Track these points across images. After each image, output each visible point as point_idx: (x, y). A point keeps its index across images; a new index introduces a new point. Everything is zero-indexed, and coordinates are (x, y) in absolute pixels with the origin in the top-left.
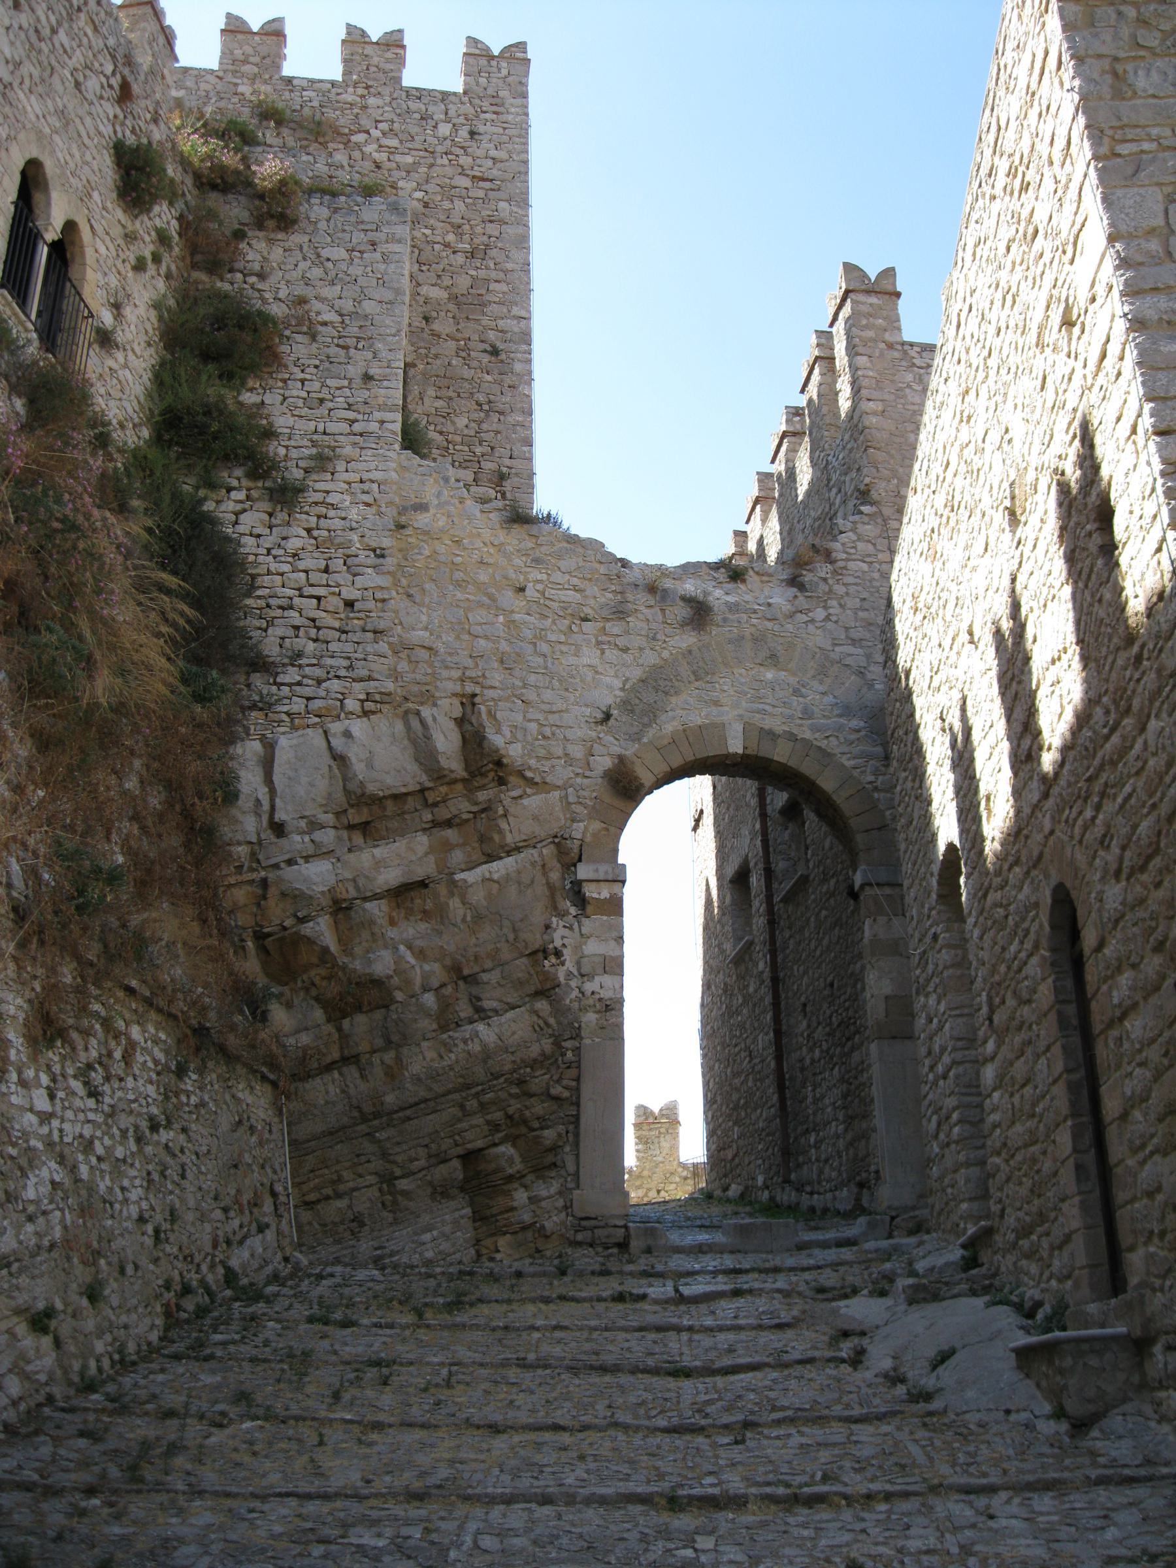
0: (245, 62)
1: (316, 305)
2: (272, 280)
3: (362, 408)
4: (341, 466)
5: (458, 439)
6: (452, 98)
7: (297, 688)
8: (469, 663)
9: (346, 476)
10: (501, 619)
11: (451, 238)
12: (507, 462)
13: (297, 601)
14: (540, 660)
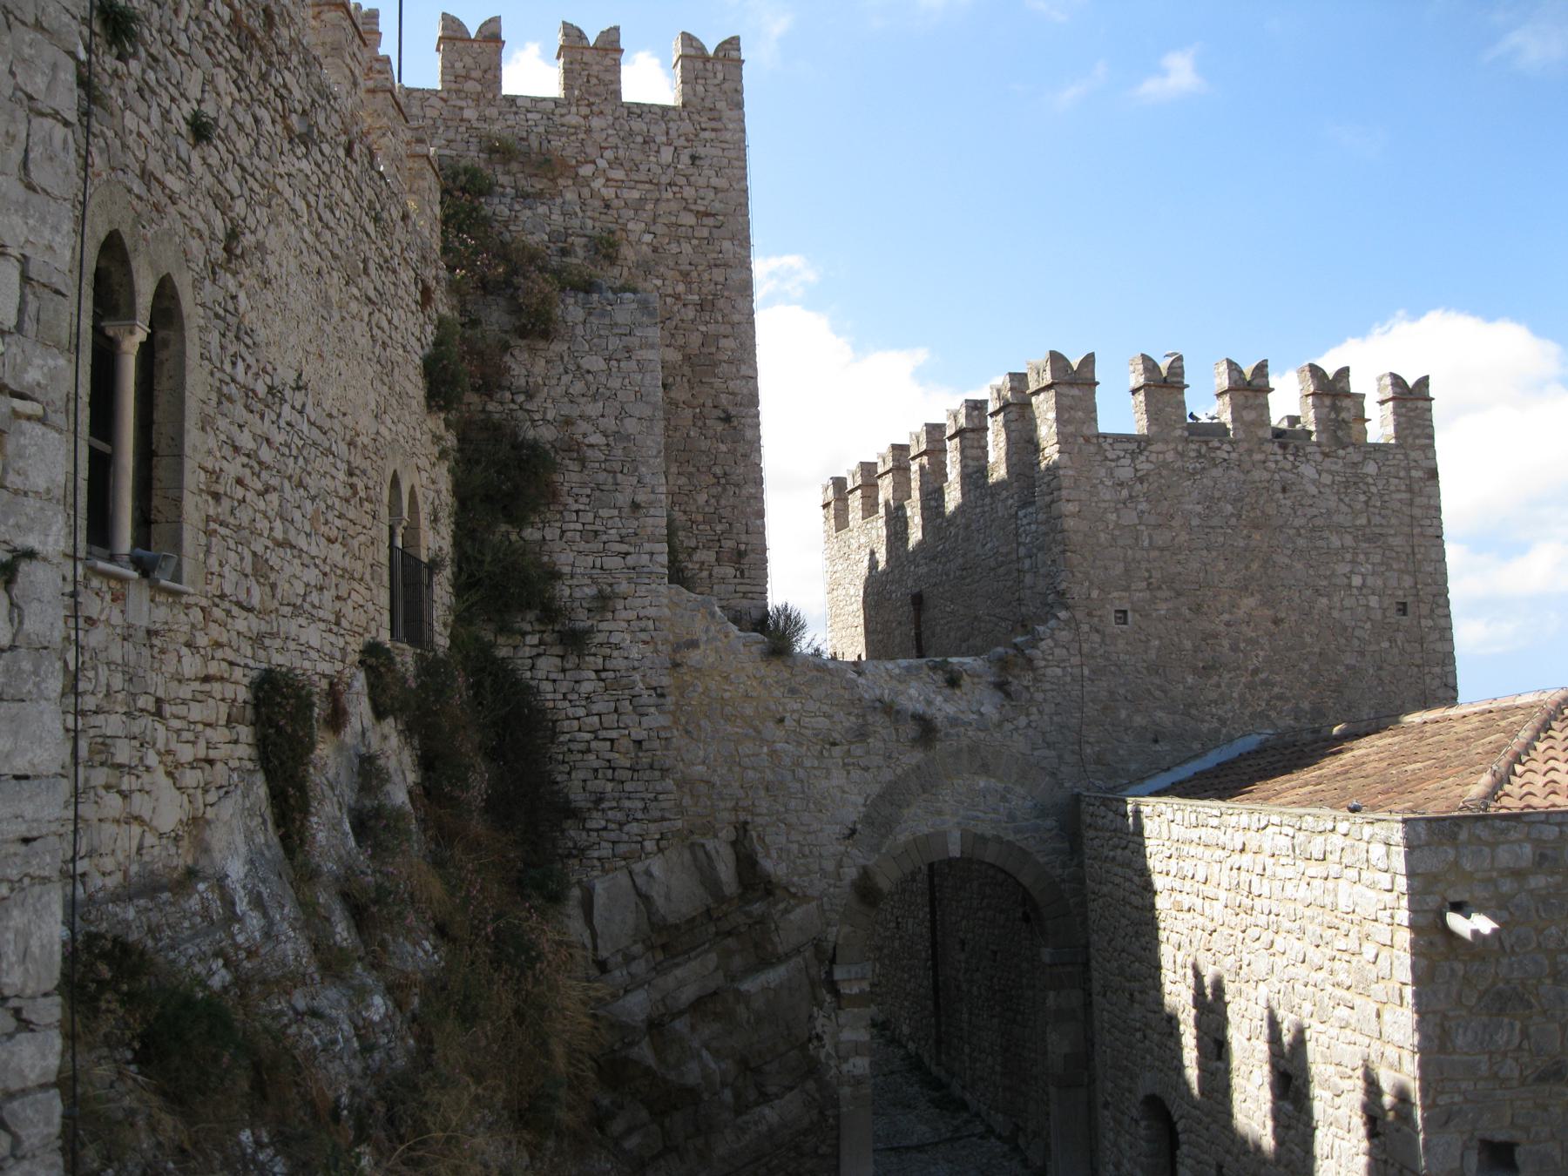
0: (467, 77)
1: (584, 426)
2: (539, 399)
3: (633, 540)
4: (620, 604)
5: (700, 518)
6: (672, 114)
7: (604, 834)
8: (741, 793)
9: (624, 615)
10: (765, 749)
11: (681, 288)
12: (744, 538)
13: (594, 745)
14: (798, 785)
